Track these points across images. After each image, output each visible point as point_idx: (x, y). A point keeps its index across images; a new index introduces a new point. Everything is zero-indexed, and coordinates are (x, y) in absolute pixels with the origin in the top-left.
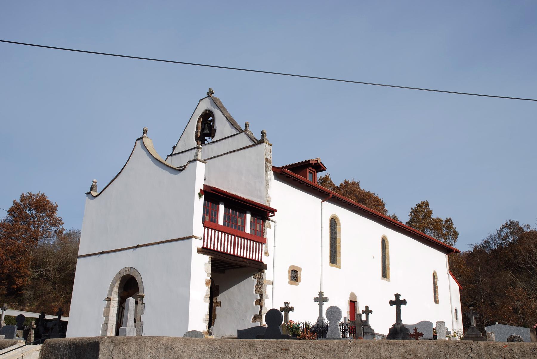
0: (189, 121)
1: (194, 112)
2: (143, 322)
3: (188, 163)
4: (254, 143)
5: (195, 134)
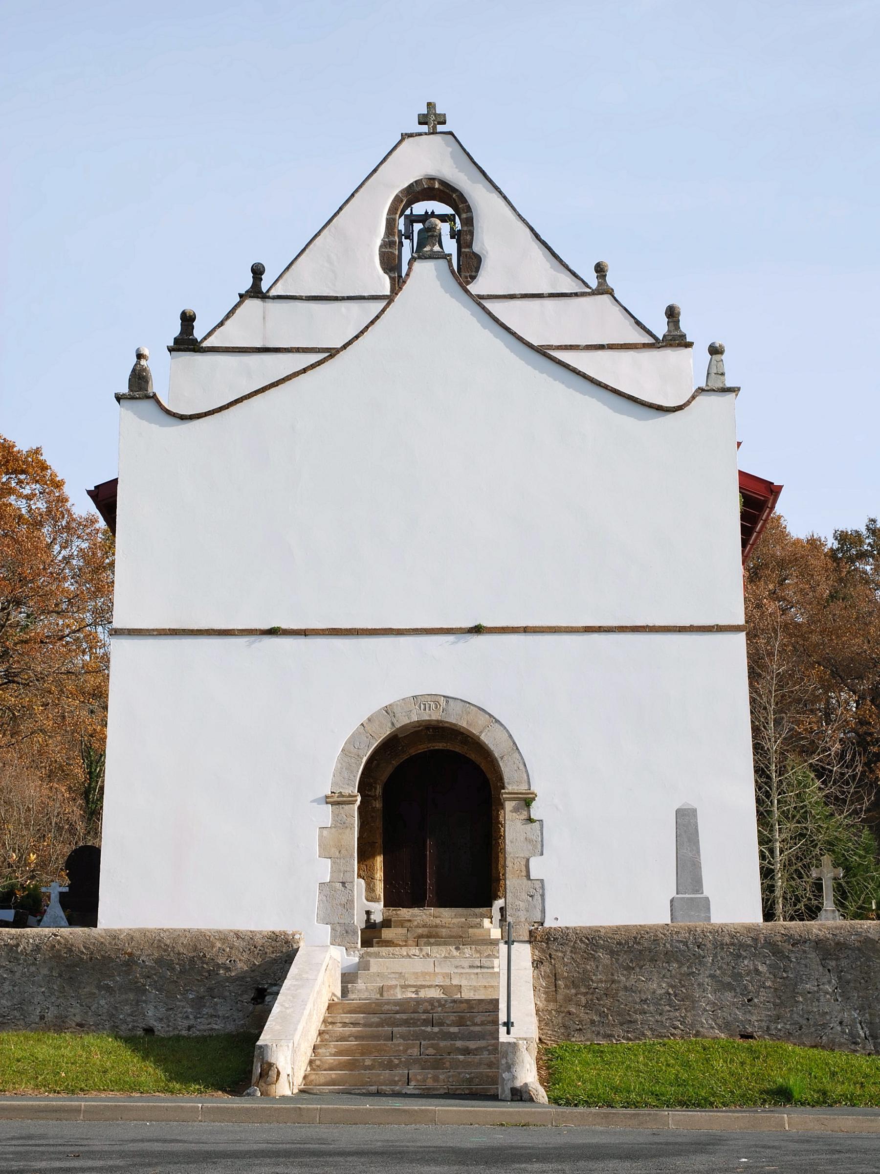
0: (353, 195)
1: (375, 171)
2: (542, 881)
3: (696, 391)
4: (654, 341)
5: (381, 247)
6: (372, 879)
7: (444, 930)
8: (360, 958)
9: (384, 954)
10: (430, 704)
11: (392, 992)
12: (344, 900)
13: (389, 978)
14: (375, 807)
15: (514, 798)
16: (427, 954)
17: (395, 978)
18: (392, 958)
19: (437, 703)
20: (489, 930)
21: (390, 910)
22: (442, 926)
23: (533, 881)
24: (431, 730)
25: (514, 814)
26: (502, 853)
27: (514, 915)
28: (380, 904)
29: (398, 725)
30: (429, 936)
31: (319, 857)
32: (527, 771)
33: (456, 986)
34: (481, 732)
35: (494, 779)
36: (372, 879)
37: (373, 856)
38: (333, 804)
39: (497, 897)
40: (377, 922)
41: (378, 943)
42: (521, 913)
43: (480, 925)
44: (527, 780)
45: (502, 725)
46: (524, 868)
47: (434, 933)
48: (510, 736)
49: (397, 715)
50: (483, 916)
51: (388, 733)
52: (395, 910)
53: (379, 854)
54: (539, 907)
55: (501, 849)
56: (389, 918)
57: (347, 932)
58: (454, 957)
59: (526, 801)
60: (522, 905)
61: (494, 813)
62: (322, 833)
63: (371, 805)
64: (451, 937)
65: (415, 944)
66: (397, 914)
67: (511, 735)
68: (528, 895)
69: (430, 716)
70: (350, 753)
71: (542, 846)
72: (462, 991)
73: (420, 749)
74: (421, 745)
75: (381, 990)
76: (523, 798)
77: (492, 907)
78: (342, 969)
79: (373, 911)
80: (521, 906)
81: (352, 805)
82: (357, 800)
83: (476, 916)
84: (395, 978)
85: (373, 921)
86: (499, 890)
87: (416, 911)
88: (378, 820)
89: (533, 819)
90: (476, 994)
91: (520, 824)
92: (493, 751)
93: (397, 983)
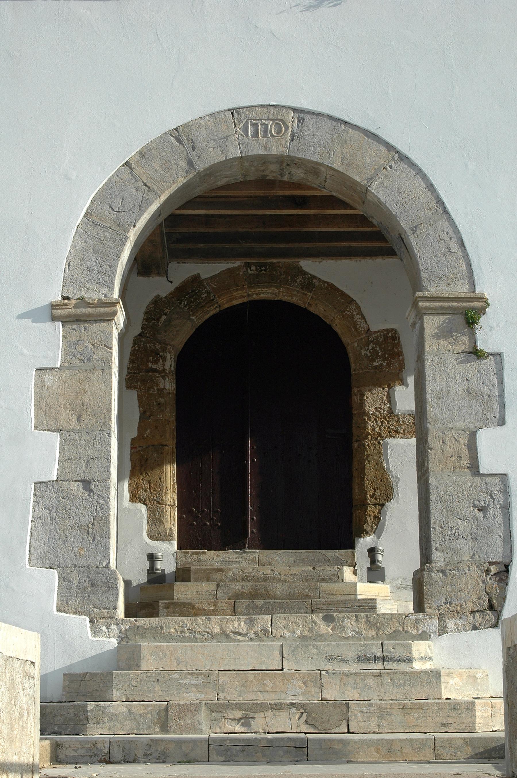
2: (504, 477)
6: (159, 503)
7: (279, 585)
8: (121, 639)
9: (172, 630)
10: (267, 125)
11: (189, 721)
12: (86, 518)
13: (183, 685)
14: (164, 388)
15: (442, 308)
16: (265, 631)
17: (196, 686)
18: (189, 640)
19: (280, 123)
20: (354, 585)
21: (188, 553)
22: (274, 579)
23: (488, 479)
24: (253, 268)
25: (442, 342)
26: (369, 462)
27: (448, 548)
28: (172, 544)
29: (201, 166)
30: (253, 596)
31: (36, 428)
32: (466, 257)
33: (336, 705)
34: (371, 179)
35: (356, 344)
36: (159, 503)
37: (160, 464)
38: (66, 320)
39: (362, 532)
40: (166, 573)
41: (167, 607)
42: (461, 544)
43: (338, 578)
44: (466, 274)
45: (413, 165)
46: (464, 452)
47: (262, 590)
48: (431, 187)
49: (198, 146)
50: (341, 563)
51: (181, 181)
52: (197, 553)
53: (171, 462)
54: (499, 531)
55: (368, 456)
56: (187, 566)
57: (93, 585)
58: (321, 637)
59: (466, 314)
60: (463, 527)
61: (355, 399)
62: (44, 379)
63: (158, 385)
64: (290, 597)
65: (230, 608)
66: (199, 561)
67: (432, 185)
68: (475, 506)
69: (267, 147)
70: (102, 219)
71: (502, 406)
72: (352, 718)
73: (235, 298)
74: (237, 290)
75: (163, 714)
76: (461, 308)
77: (354, 549)
78: (44, 679)
79: (160, 554)
80: (462, 529)
81: (105, 324)
82: (115, 313)
83: (328, 562)
84: (196, 686)
85: (159, 571)
86: (366, 522)
87: (230, 555)
88: (168, 410)
89: (482, 351)
90: (384, 723)
91: (455, 363)
92: (395, 216)
93: (200, 696)
